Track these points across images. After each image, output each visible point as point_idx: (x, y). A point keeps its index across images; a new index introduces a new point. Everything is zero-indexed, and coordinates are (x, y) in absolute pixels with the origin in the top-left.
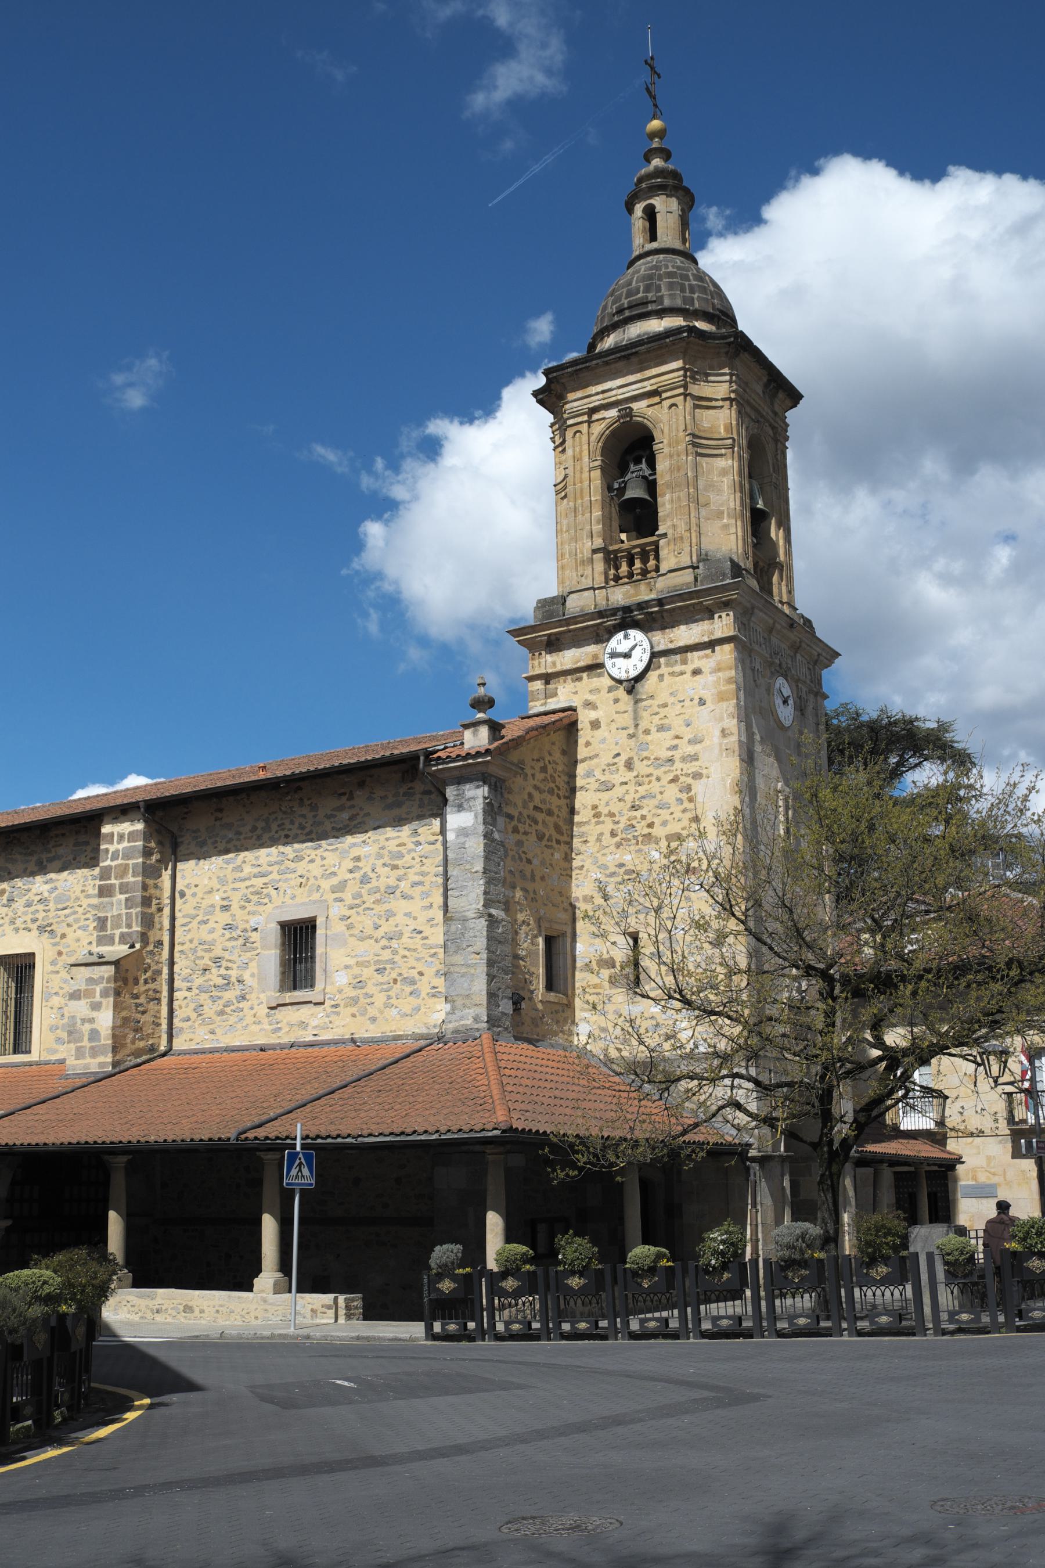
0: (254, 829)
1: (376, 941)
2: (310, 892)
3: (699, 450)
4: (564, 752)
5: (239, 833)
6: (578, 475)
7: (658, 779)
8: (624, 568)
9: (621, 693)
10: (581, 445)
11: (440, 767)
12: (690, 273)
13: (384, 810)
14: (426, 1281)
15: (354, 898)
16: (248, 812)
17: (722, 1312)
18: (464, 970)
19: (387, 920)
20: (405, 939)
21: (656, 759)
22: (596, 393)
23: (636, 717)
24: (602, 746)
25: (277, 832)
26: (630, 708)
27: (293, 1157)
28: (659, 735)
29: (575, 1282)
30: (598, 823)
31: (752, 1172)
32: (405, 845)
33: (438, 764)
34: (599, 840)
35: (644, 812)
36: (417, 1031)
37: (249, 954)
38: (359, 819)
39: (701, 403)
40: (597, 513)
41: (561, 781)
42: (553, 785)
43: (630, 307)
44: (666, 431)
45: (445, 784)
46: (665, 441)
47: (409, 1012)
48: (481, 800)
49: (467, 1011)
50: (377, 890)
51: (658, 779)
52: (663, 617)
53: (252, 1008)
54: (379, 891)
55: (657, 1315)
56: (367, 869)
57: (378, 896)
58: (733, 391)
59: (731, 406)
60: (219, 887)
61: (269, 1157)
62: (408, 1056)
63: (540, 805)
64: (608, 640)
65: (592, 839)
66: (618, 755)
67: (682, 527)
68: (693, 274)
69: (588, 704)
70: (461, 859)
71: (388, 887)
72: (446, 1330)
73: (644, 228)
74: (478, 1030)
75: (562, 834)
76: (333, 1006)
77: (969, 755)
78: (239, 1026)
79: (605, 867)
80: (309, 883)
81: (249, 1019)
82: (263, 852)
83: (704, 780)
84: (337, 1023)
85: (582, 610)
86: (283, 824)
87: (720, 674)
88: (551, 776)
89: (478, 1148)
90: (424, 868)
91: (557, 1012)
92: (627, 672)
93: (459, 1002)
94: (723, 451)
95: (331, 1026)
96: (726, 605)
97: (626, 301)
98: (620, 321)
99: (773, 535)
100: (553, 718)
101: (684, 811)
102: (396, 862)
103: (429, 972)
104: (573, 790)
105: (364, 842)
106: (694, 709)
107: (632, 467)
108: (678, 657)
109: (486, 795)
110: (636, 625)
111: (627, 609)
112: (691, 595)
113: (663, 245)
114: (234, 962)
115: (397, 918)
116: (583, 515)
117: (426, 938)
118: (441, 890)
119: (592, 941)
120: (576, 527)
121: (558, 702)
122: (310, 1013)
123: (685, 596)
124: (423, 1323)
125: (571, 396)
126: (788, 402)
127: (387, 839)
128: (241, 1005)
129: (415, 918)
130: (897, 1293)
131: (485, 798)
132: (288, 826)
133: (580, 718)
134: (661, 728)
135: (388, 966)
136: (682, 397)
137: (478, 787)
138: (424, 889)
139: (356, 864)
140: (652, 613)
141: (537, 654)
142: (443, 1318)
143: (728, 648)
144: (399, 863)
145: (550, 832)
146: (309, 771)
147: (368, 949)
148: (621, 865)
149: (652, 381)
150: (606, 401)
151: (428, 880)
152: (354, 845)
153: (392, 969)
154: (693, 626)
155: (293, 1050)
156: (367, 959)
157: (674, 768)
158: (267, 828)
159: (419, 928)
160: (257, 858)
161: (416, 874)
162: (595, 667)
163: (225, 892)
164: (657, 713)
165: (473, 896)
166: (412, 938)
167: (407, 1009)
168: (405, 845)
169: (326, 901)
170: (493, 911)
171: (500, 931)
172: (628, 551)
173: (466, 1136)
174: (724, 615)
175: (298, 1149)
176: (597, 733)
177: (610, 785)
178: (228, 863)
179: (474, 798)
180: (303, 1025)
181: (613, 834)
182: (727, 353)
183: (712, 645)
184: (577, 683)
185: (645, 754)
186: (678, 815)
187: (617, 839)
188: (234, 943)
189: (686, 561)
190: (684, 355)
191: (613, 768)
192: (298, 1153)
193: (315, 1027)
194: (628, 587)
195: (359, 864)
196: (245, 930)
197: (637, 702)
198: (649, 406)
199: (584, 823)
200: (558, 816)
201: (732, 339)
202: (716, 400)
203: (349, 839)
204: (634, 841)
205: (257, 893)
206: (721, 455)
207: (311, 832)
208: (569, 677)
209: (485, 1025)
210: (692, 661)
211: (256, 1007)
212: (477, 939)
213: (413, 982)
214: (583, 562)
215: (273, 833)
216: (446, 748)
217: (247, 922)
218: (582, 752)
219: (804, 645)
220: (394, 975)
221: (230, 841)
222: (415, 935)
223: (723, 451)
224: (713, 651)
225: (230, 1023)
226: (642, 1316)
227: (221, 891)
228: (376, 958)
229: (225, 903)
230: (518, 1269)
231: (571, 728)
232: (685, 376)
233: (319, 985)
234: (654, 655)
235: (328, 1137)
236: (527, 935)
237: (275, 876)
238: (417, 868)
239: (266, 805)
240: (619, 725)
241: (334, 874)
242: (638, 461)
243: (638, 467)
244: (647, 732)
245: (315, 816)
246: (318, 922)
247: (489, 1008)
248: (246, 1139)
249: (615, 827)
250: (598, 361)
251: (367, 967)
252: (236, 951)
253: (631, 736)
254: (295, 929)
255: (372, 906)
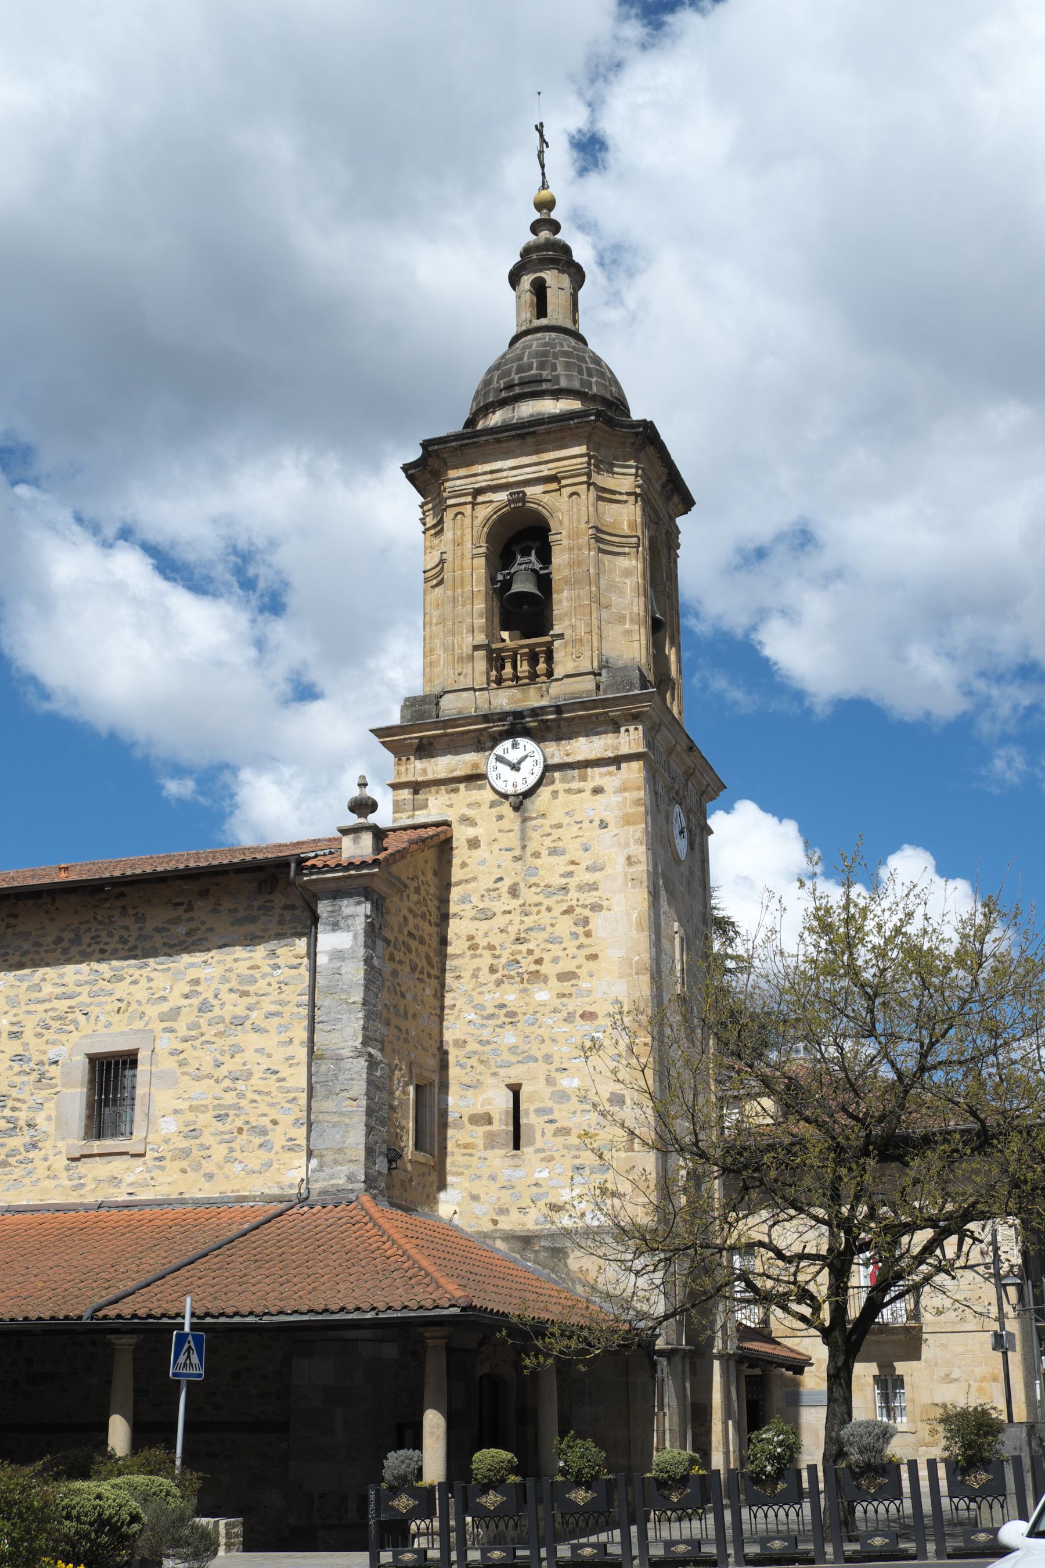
0: (59, 940)
1: (217, 1081)
2: (131, 1019)
3: (602, 546)
4: (436, 873)
5: (39, 945)
6: (458, 561)
7: (549, 909)
8: (508, 670)
9: (506, 808)
10: (462, 529)
11: (314, 877)
12: (586, 356)
13: (232, 925)
14: (372, 1497)
15: (189, 1029)
16: (51, 920)
17: (676, 1536)
18: (336, 1119)
19: (232, 1057)
20: (255, 1080)
21: (547, 886)
22: (483, 473)
23: (524, 837)
24: (481, 868)
25: (89, 945)
26: (517, 826)
27: (182, 1338)
28: (551, 859)
29: (580, 1496)
30: (474, 956)
31: (659, 1367)
32: (258, 967)
33: (311, 874)
34: (475, 976)
35: (531, 946)
36: (267, 1191)
37: (45, 1093)
38: (199, 935)
39: (605, 495)
40: (480, 606)
41: (432, 905)
42: (424, 909)
43: (521, 384)
44: (566, 520)
45: (316, 897)
46: (564, 533)
47: (257, 1168)
48: (362, 919)
49: (339, 1168)
50: (221, 1020)
51: (549, 909)
52: (559, 727)
53: (46, 1159)
54: (223, 1021)
55: (593, 1539)
56: (209, 995)
57: (221, 1027)
58: (638, 486)
59: (636, 502)
60: (7, 1008)
61: (123, 1341)
62: (269, 1221)
63: (413, 932)
64: (492, 748)
65: (467, 974)
66: (501, 879)
67: (582, 629)
68: (590, 357)
69: (465, 820)
70: (334, 987)
71: (235, 1017)
72: (401, 1561)
73: (532, 302)
74: (352, 1191)
75: (433, 967)
76: (156, 1159)
77: (733, 924)
78: (27, 1181)
79: (479, 1007)
80: (130, 1009)
81: (41, 1172)
82: (70, 969)
83: (604, 912)
84: (161, 1179)
85: (459, 713)
86: (98, 936)
87: (626, 794)
88: (424, 899)
89: (350, 1334)
90: (283, 996)
91: (424, 1174)
92: (515, 785)
93: (329, 1158)
94: (627, 550)
95: (152, 1183)
96: (635, 718)
97: (517, 377)
98: (509, 397)
99: (667, 652)
100: (431, 831)
101: (580, 947)
102: (246, 988)
103: (286, 1120)
104: (445, 917)
105: (205, 962)
106: (592, 832)
107: (519, 559)
108: (576, 772)
109: (369, 913)
110: (527, 733)
111: (518, 715)
112: (595, 704)
113: (553, 323)
114: (24, 1102)
115: (245, 1054)
116: (463, 606)
117: (283, 1080)
118: (306, 1023)
119: (464, 1093)
120: (454, 619)
121: (429, 815)
122: (125, 1166)
123: (589, 705)
124: (368, 1553)
125: (452, 473)
126: (681, 507)
127: (236, 960)
128: (30, 1155)
129: (269, 1056)
130: (792, 1513)
131: (367, 917)
132: (104, 939)
133: (456, 835)
134: (553, 852)
135: (231, 1112)
136: (585, 486)
137: (359, 903)
138: (282, 1021)
139: (194, 988)
140: (547, 720)
141: (404, 759)
142: (395, 1545)
143: (636, 766)
144: (251, 988)
145: (422, 963)
146: (144, 873)
147: (205, 1091)
148: (502, 1006)
149: (550, 466)
150: (494, 482)
151: (287, 1010)
152: (192, 965)
153: (237, 1115)
154: (595, 738)
155: (102, 1211)
156: (203, 1102)
157: (568, 898)
158: (77, 940)
159: (274, 1068)
160: (61, 976)
161: (272, 1003)
162: (476, 778)
163: (15, 1015)
164: (549, 835)
165: (349, 1031)
166: (265, 1079)
167: (255, 1165)
168: (258, 967)
169: (151, 1031)
170: (370, 1049)
171: (378, 1074)
172: (515, 652)
173: (413, 1314)
174: (631, 728)
175: (187, 1329)
176: (476, 853)
177: (489, 913)
178: (21, 980)
179: (353, 916)
180: (115, 1181)
181: (493, 970)
182: (633, 444)
183: (617, 761)
184: (452, 795)
185: (533, 880)
186: (572, 951)
187: (498, 975)
188: (25, 1078)
189: (585, 666)
190: (588, 441)
191: (494, 894)
192: (187, 1335)
193: (131, 1184)
194: (514, 691)
195: (198, 988)
196: (41, 1063)
197: (524, 820)
198: (544, 493)
199: (457, 956)
200: (429, 946)
201: (641, 429)
202: (621, 494)
203: (186, 958)
204: (519, 979)
205: (60, 1018)
206: (624, 554)
207: (135, 947)
208: (443, 788)
209: (362, 1185)
210: (593, 778)
211: (51, 1157)
212: (356, 1082)
213: (264, 1132)
214: (461, 659)
215: (84, 947)
216: (316, 856)
217: (44, 1052)
218: (457, 874)
219: (697, 772)
220: (239, 1123)
221: (25, 954)
222: (268, 1075)
223: (627, 550)
224: (619, 768)
225: (15, 1177)
226: (575, 1541)
227: (11, 1014)
228: (216, 1102)
229: (15, 1029)
230: (503, 1480)
231: (444, 847)
232: (589, 463)
233: (139, 1133)
234: (548, 768)
235: (222, 1315)
236: (399, 1082)
237: (84, 998)
238: (275, 996)
239: (76, 912)
240: (503, 846)
241: (164, 999)
242: (526, 553)
243: (526, 559)
244: (537, 855)
245: (141, 929)
246: (140, 1056)
247: (367, 1167)
248: (105, 1317)
249: (495, 962)
250: (489, 437)
251: (203, 1112)
252: (27, 1089)
253: (517, 859)
254: (109, 1064)
255: (213, 1039)
